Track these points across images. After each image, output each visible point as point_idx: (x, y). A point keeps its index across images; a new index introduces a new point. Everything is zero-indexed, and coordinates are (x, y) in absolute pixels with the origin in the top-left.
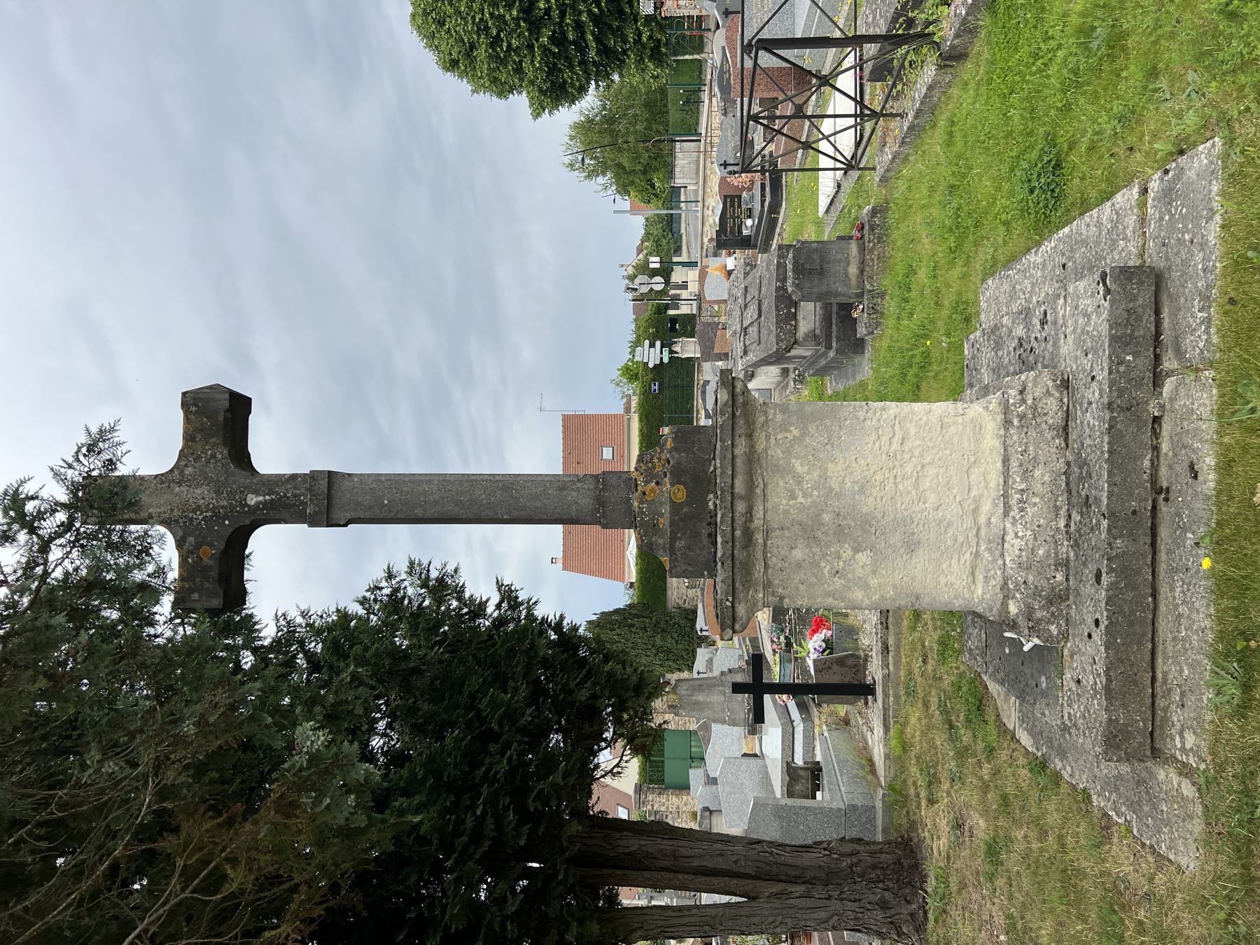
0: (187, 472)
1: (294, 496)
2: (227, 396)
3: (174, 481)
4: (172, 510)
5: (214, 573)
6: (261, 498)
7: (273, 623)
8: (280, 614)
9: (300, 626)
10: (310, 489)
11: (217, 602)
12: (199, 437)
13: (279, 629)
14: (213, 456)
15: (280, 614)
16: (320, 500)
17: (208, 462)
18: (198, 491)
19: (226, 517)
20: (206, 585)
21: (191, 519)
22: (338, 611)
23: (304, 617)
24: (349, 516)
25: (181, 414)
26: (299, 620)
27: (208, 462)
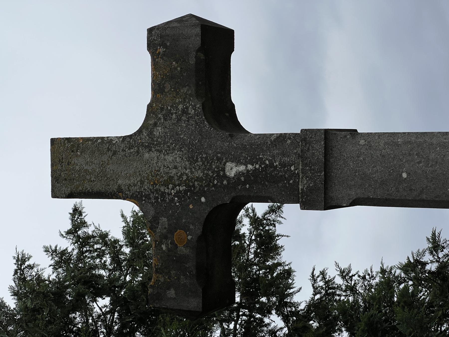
0: (156, 133)
1: (283, 165)
2: (198, 30)
3: (142, 145)
4: (142, 182)
5: (191, 265)
6: (242, 168)
7: (310, 284)
8: (317, 273)
9: (339, 287)
10: (301, 156)
11: (194, 303)
12: (168, 87)
13: (316, 291)
14: (185, 111)
15: (317, 273)
16: (325, 169)
17: (179, 120)
18: (170, 158)
19: (203, 194)
20: (183, 280)
21: (163, 194)
22: (383, 271)
23: (343, 277)
24: (353, 194)
25: (148, 57)
26: (339, 281)
27: (179, 120)
